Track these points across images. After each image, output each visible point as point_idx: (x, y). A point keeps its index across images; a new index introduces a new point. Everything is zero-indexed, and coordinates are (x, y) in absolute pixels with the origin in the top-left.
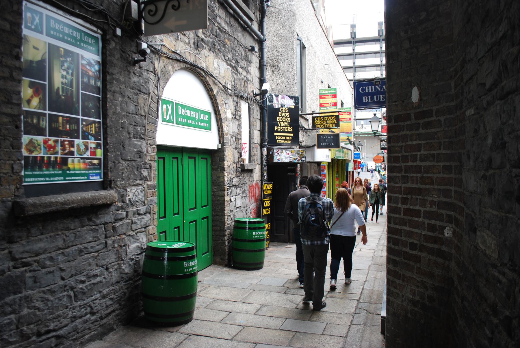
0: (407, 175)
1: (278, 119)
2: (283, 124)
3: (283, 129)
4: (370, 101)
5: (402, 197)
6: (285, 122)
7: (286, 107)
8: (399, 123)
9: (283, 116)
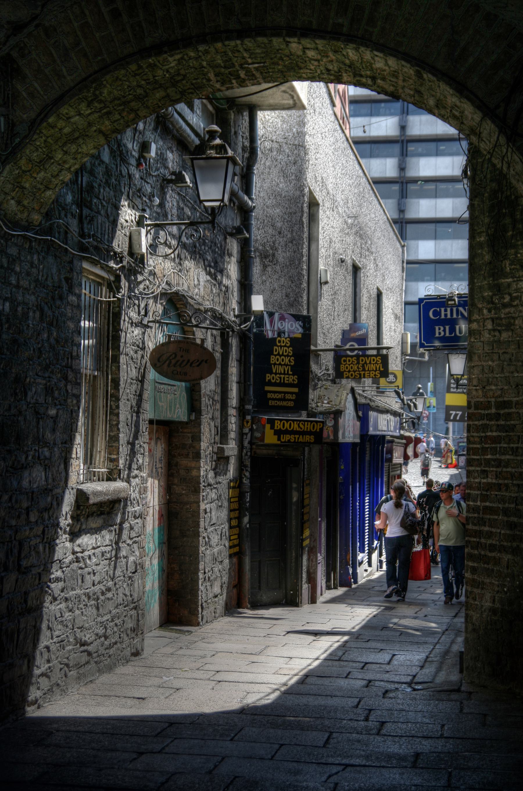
0: (486, 469)
1: (273, 359)
2: (281, 369)
3: (280, 378)
4: (447, 334)
5: (481, 494)
6: (285, 365)
7: (286, 336)
8: (480, 411)
9: (281, 353)
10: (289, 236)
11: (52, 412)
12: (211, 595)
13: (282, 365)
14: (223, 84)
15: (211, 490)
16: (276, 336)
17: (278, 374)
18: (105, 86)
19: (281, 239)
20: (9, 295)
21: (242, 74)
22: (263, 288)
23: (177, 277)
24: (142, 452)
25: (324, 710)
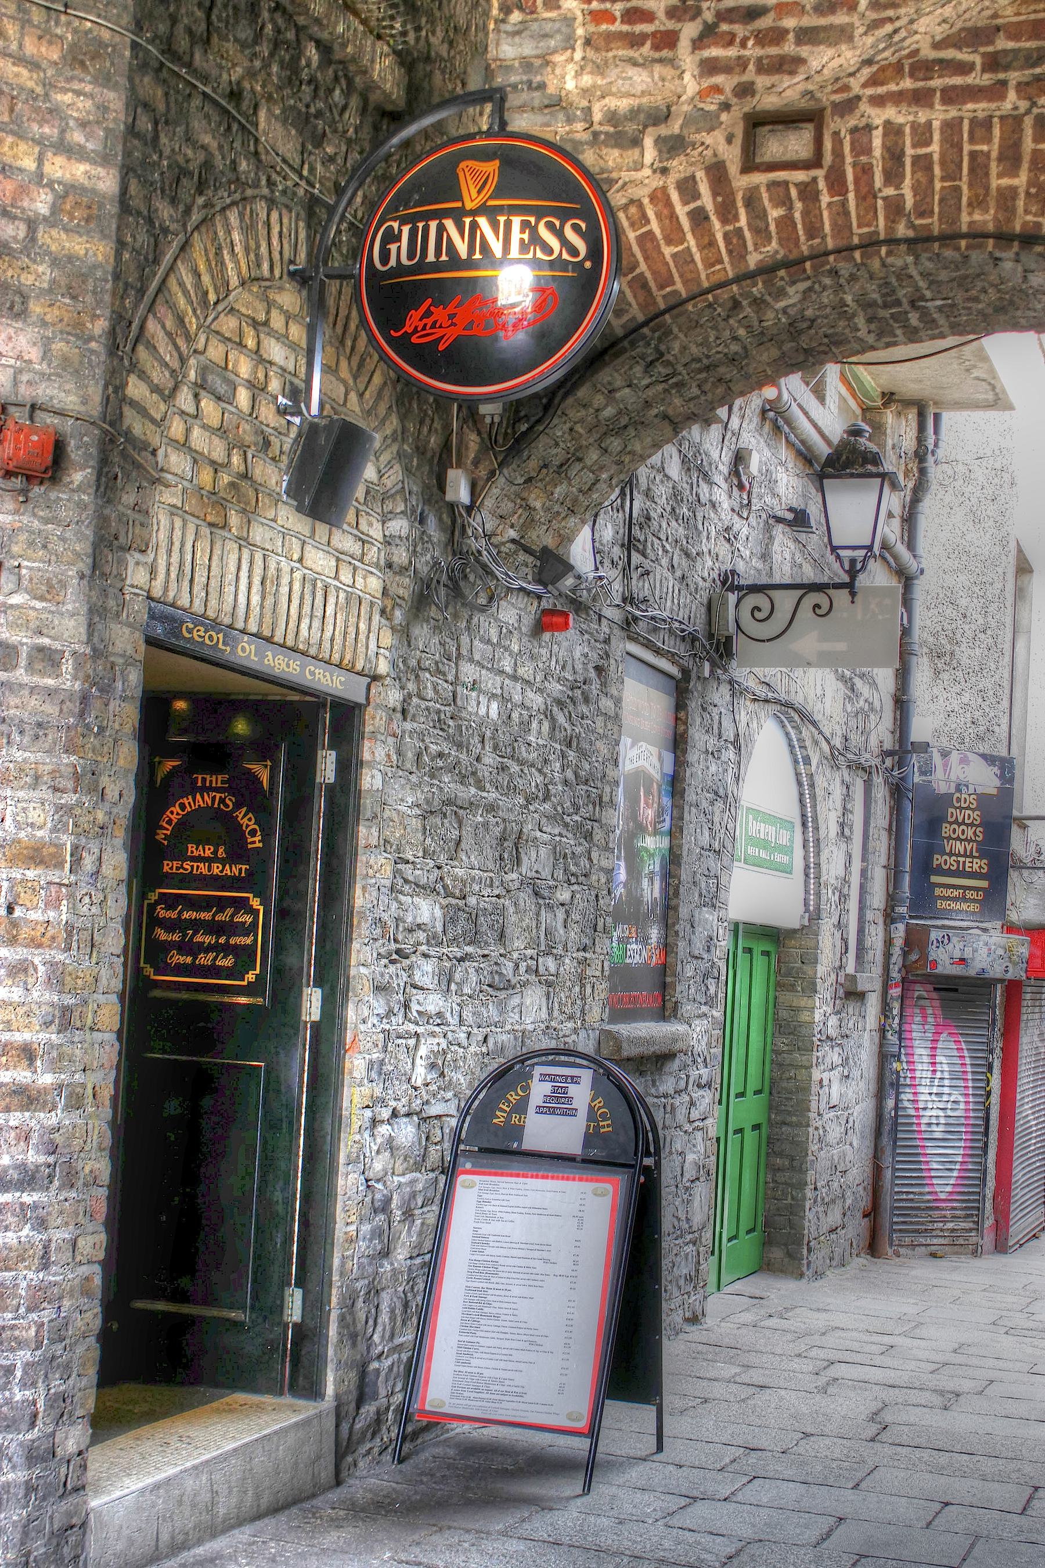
1: (946, 830)
2: (959, 847)
6: (966, 840)
10: (981, 621)
11: (564, 895)
12: (824, 1229)
13: (961, 840)
14: (880, 335)
15: (832, 1047)
16: (952, 790)
17: (955, 855)
18: (676, 337)
19: (966, 627)
20: (499, 691)
21: (914, 319)
22: (933, 709)
23: (785, 681)
24: (716, 974)
25: (1022, 1444)
